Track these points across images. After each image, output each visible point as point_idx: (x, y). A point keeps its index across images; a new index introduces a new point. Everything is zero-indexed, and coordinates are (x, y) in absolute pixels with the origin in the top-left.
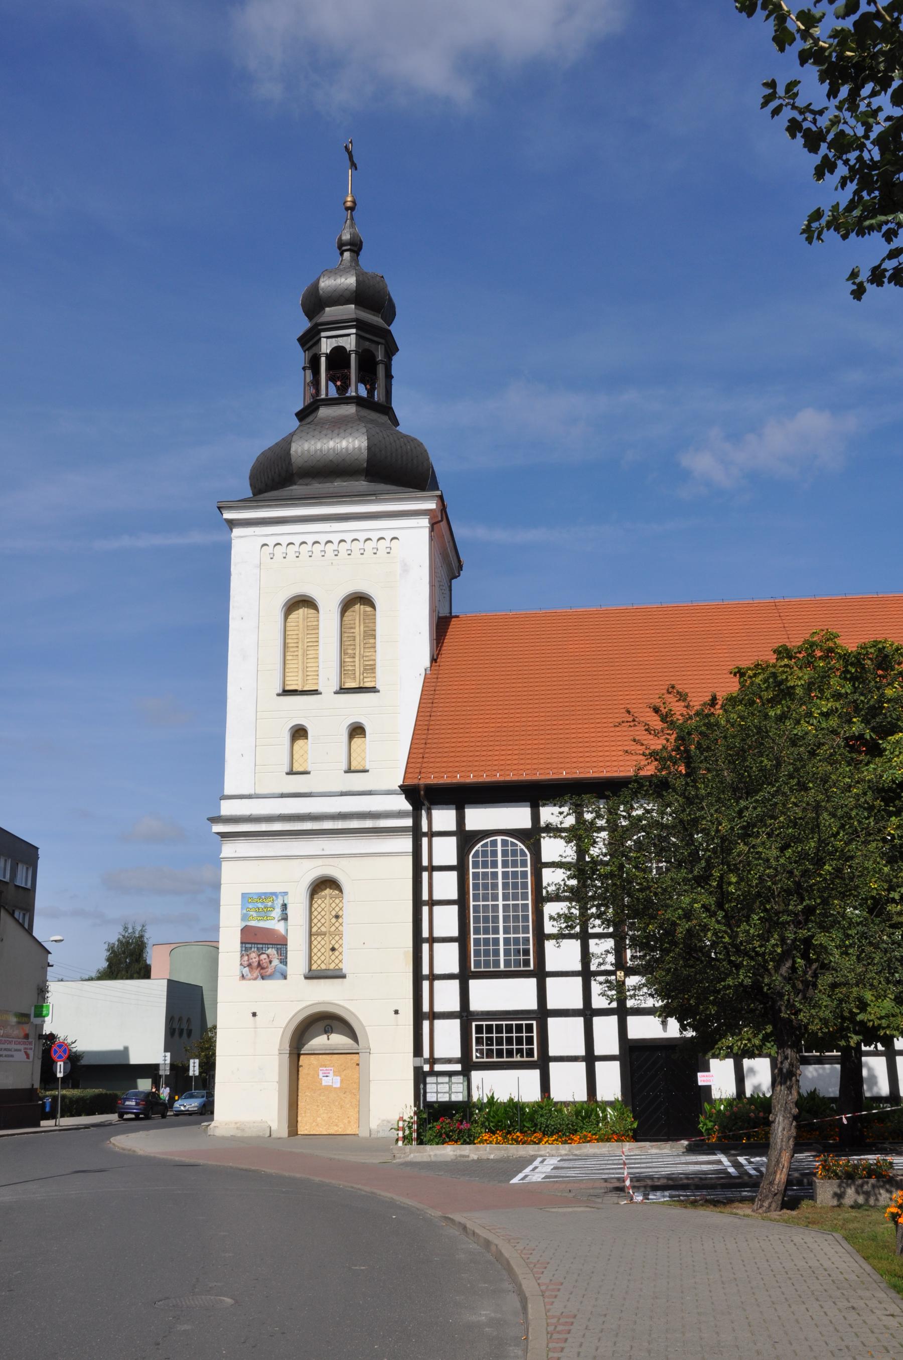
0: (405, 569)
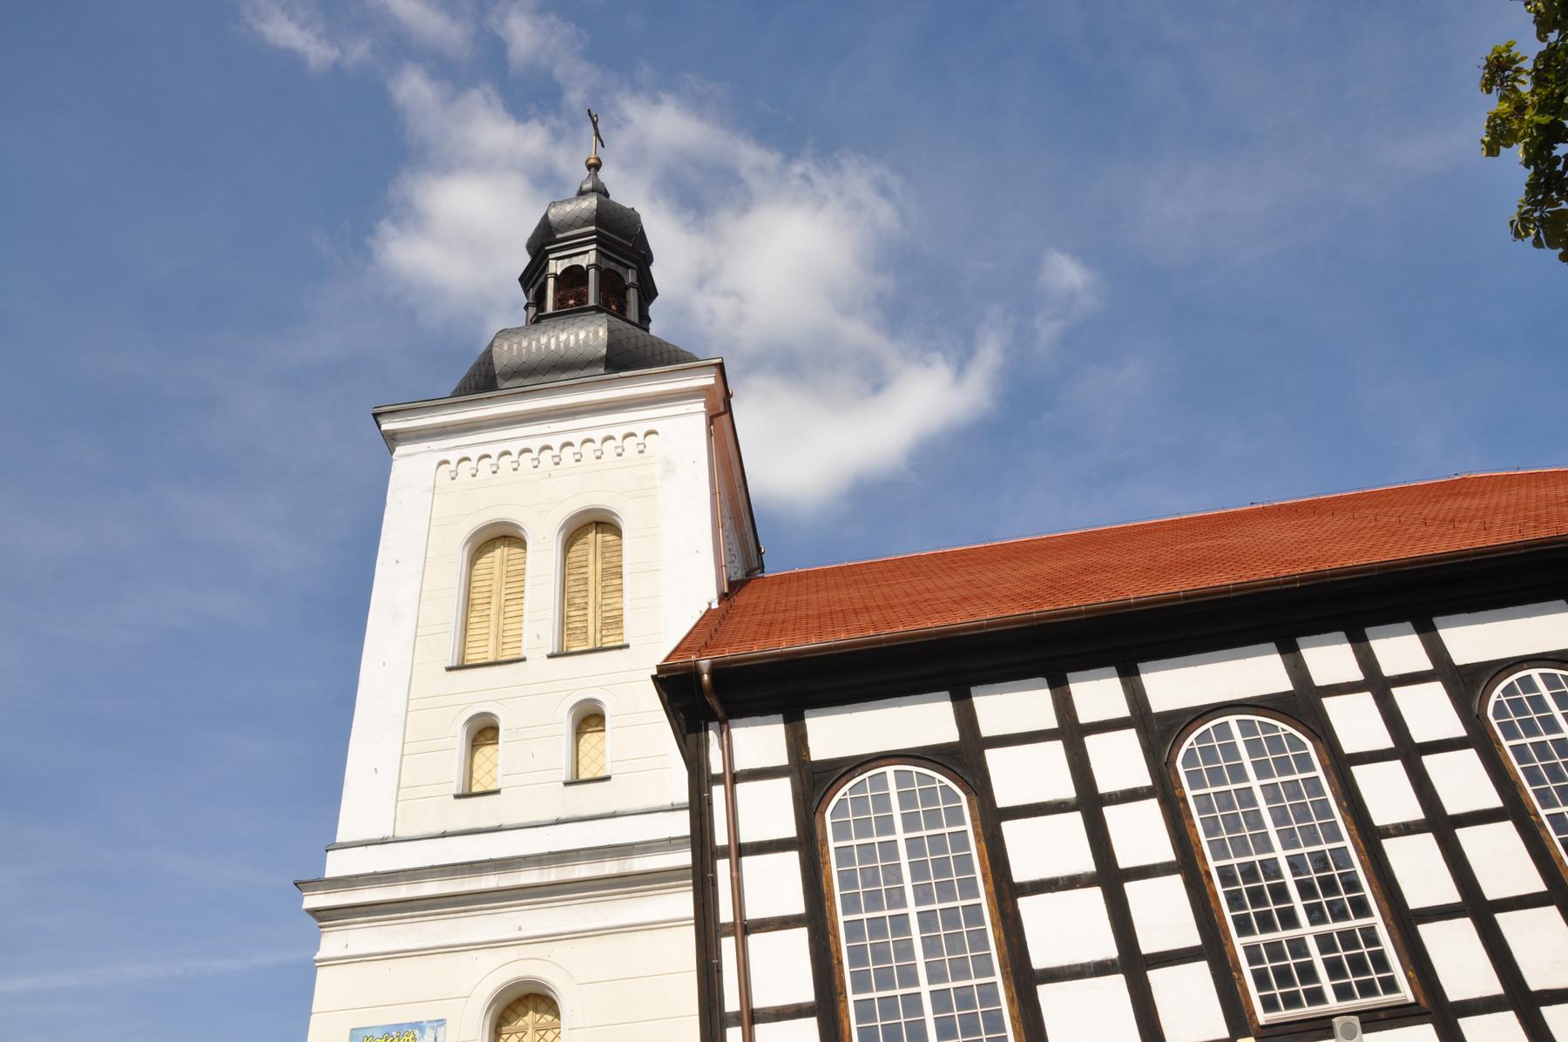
0: (669, 468)
